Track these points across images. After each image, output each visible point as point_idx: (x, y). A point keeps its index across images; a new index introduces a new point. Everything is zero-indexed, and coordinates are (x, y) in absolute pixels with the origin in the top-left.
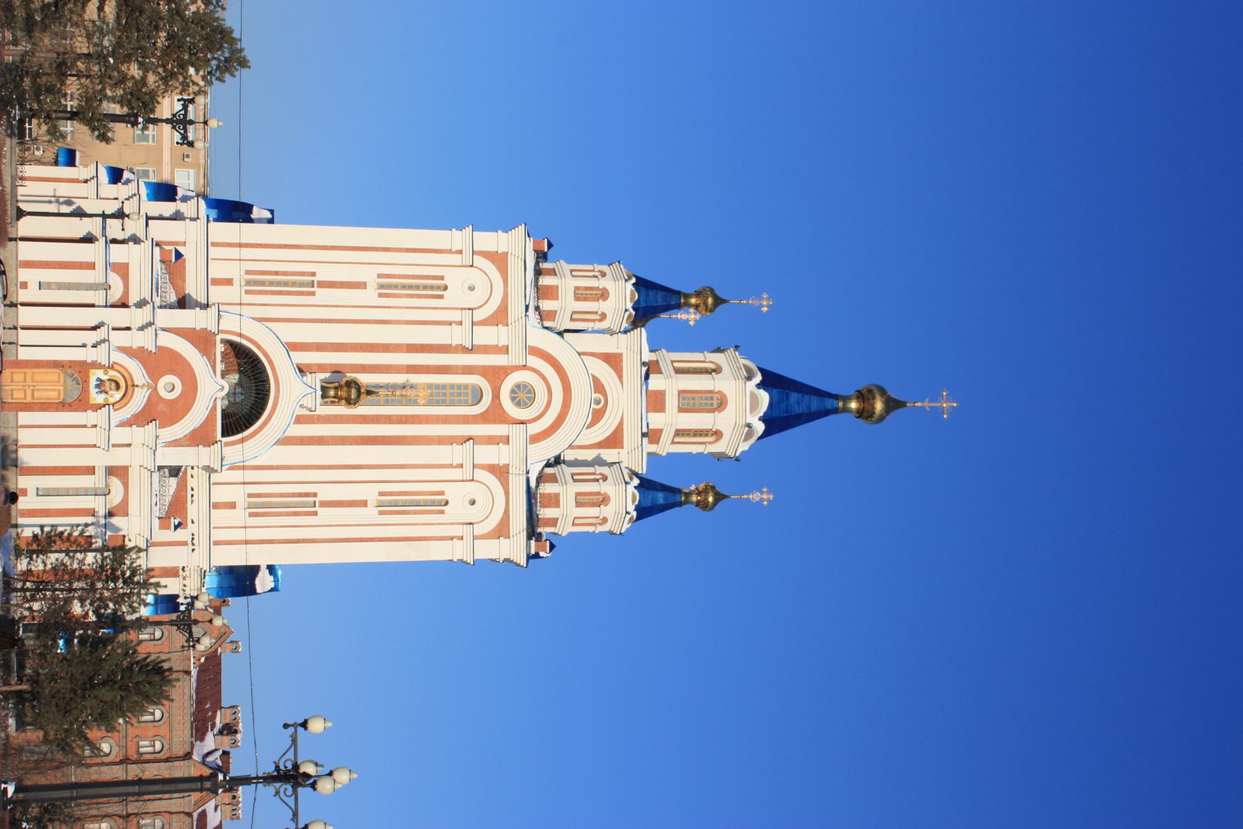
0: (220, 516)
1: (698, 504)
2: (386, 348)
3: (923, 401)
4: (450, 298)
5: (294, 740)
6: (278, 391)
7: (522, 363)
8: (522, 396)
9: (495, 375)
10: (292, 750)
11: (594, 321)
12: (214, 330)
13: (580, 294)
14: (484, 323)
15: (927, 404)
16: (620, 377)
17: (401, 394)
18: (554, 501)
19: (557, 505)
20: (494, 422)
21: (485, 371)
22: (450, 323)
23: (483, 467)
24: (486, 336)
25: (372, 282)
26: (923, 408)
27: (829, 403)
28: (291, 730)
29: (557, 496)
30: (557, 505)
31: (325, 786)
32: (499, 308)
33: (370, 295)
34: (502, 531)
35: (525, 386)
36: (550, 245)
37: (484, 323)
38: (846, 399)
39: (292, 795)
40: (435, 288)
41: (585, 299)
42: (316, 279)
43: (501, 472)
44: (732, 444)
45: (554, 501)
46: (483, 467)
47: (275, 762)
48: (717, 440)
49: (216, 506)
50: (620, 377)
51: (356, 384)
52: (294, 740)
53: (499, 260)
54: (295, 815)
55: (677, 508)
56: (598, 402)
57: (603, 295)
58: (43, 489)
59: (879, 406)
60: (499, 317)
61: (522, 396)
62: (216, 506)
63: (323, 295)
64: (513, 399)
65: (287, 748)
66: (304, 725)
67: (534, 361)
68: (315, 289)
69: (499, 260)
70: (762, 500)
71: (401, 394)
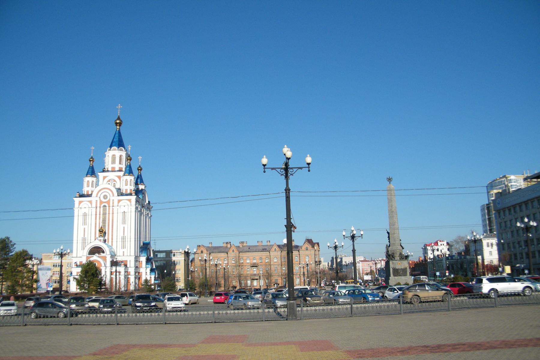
0: (125, 254)
1: (130, 161)
2: (96, 224)
3: (118, 112)
4: (87, 212)
5: (346, 237)
6: (101, 246)
7: (99, 198)
8: (105, 197)
9: (101, 202)
10: (277, 169)
11: (132, 182)
12: (86, 256)
13: (88, 186)
14: (91, 205)
15: (119, 111)
16: (107, 176)
17: (104, 221)
18: (126, 190)
19: (127, 189)
20: (110, 202)
21: (100, 205)
22: (92, 212)
23: (79, 205)
24: (94, 205)
25: (123, 226)
26: (120, 112)
27: (117, 132)
28: (345, 238)
29: (126, 189)
30: (127, 189)
31: (355, 232)
32: (80, 203)
33: (126, 226)
34: (130, 200)
35: (104, 198)
36: (78, 192)
37: (91, 205)
38: (117, 129)
39: (293, 170)
40: (85, 215)
41: (89, 185)
42: (83, 237)
43: (119, 201)
44: (124, 154)
45: (126, 190)
46: (79, 205)
47: (281, 176)
48: (122, 155)
49: (124, 255)
50: (107, 176)
51: (99, 230)
52: (346, 237)
53: (80, 202)
54: (360, 237)
55: (131, 165)
56: (112, 181)
57: (88, 181)
58: (70, 286)
59: (118, 121)
60: (90, 202)
61: (105, 197)
62: (124, 255)
63: (86, 236)
64: (107, 198)
65: (276, 171)
66: (344, 236)
67: (99, 196)
68: (85, 237)
69: (80, 202)
70: (130, 147)
71: (104, 221)
